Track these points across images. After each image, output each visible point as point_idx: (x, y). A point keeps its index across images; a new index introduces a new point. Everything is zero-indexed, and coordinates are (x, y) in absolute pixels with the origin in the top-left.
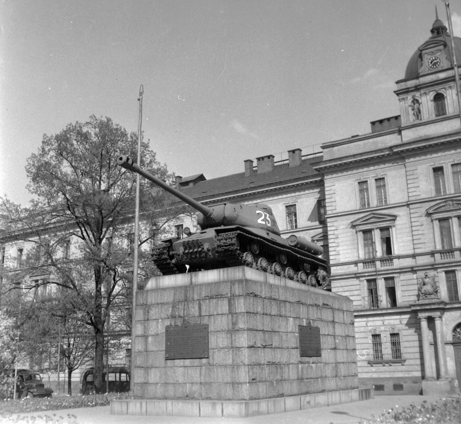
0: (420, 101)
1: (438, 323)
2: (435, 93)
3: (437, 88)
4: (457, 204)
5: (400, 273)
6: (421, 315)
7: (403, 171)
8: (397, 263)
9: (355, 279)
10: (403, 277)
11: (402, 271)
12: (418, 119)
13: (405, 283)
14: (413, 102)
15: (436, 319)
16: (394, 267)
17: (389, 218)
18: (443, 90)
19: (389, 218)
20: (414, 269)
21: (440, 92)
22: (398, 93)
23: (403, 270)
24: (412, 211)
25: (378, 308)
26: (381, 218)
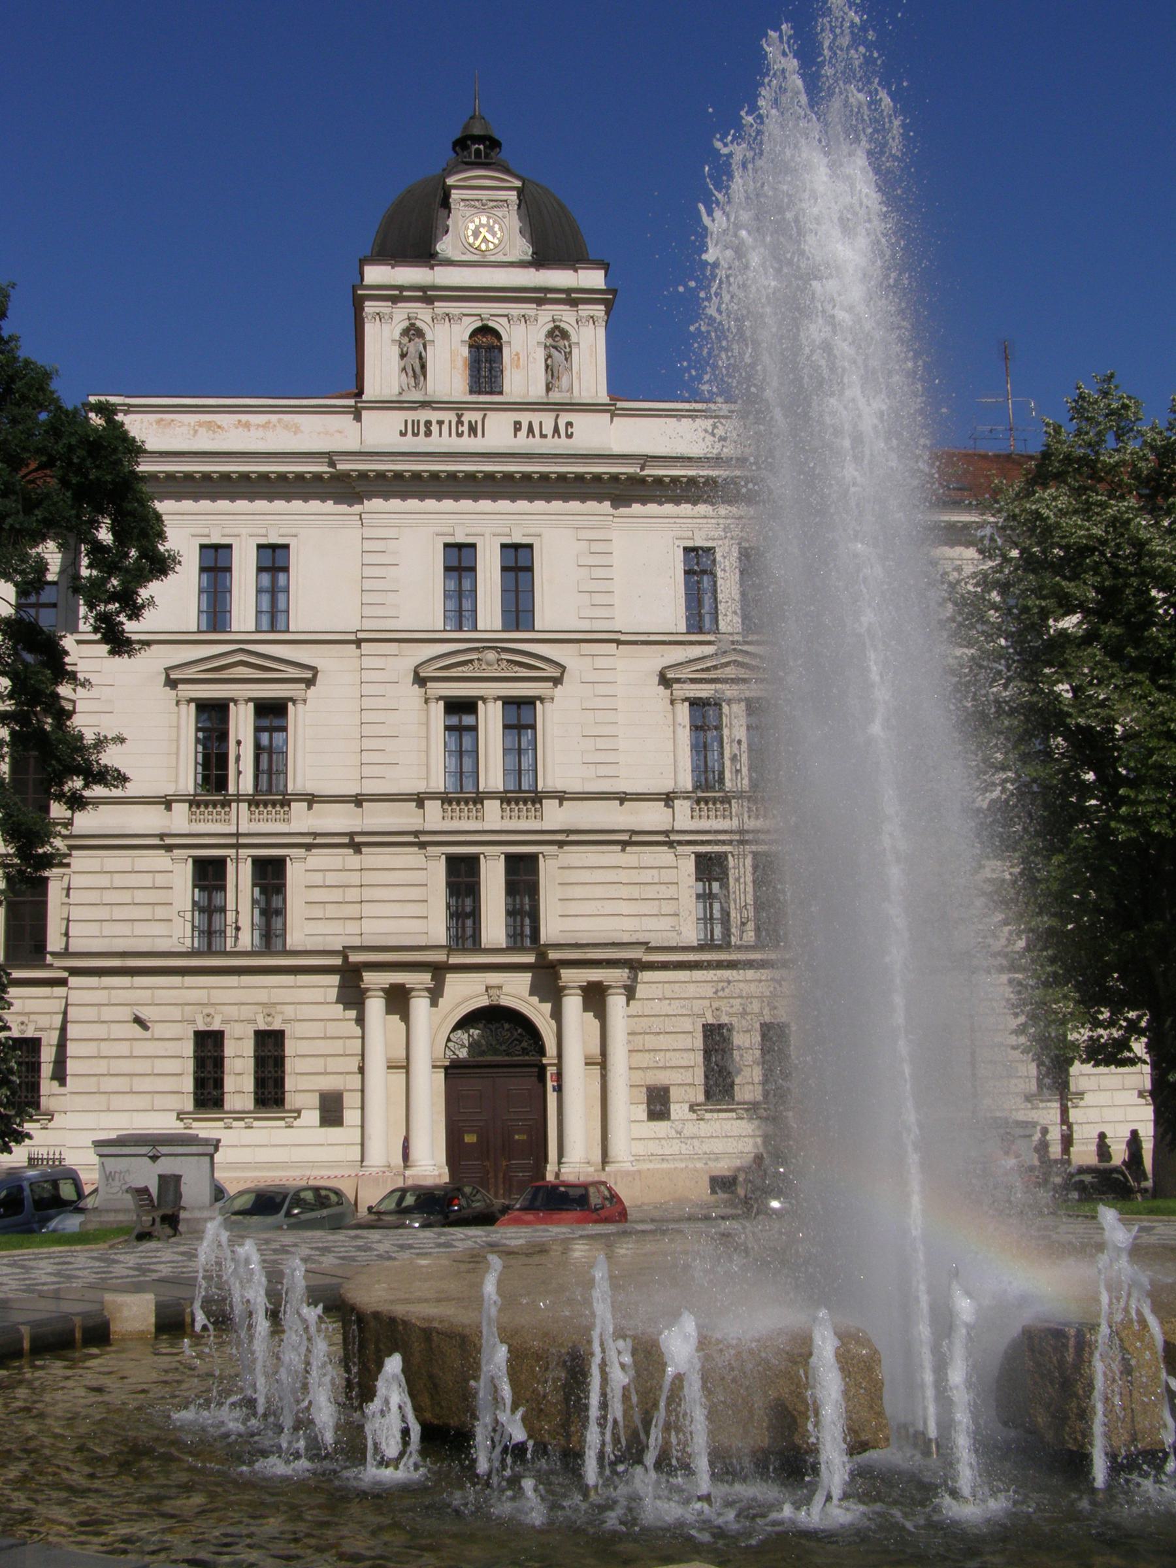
0: (429, 337)
1: (616, 1003)
2: (479, 324)
3: (485, 309)
4: (508, 661)
5: (309, 847)
6: (568, 976)
7: (353, 534)
8: (301, 819)
9: (665, 848)
10: (318, 859)
11: (313, 842)
12: (416, 385)
13: (317, 878)
14: (405, 332)
15: (611, 991)
16: (546, 826)
17: (294, 673)
18: (504, 321)
19: (294, 673)
20: (358, 839)
21: (491, 324)
23: (319, 840)
24: (367, 662)
25: (475, 945)
26: (266, 668)
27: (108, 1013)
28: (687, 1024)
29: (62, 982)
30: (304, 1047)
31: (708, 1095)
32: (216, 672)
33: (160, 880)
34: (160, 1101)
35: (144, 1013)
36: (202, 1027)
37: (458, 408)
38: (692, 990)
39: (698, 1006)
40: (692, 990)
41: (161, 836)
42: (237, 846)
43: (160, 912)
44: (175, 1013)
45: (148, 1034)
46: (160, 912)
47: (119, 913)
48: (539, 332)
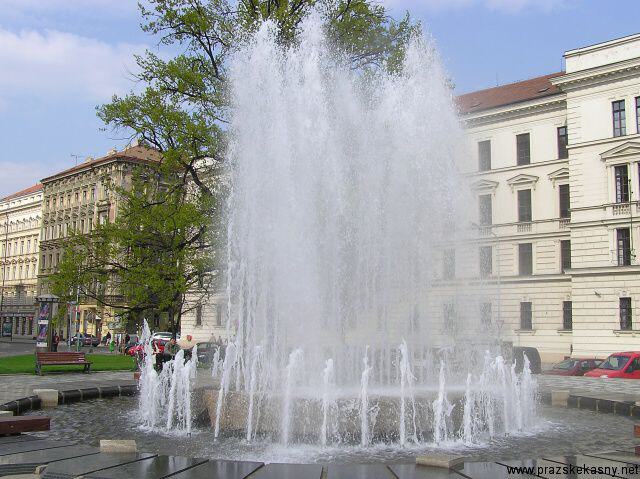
10: (542, 243)
27: (587, 291)
28: (557, 301)
29: (570, 280)
30: (537, 308)
31: (622, 328)
32: (619, 153)
33: (604, 239)
34: (607, 326)
35: (599, 291)
36: (622, 296)
38: (560, 289)
39: (562, 295)
40: (560, 289)
41: (602, 221)
42: (632, 222)
43: (604, 252)
44: (611, 291)
45: (601, 299)
46: (604, 252)
47: (589, 252)
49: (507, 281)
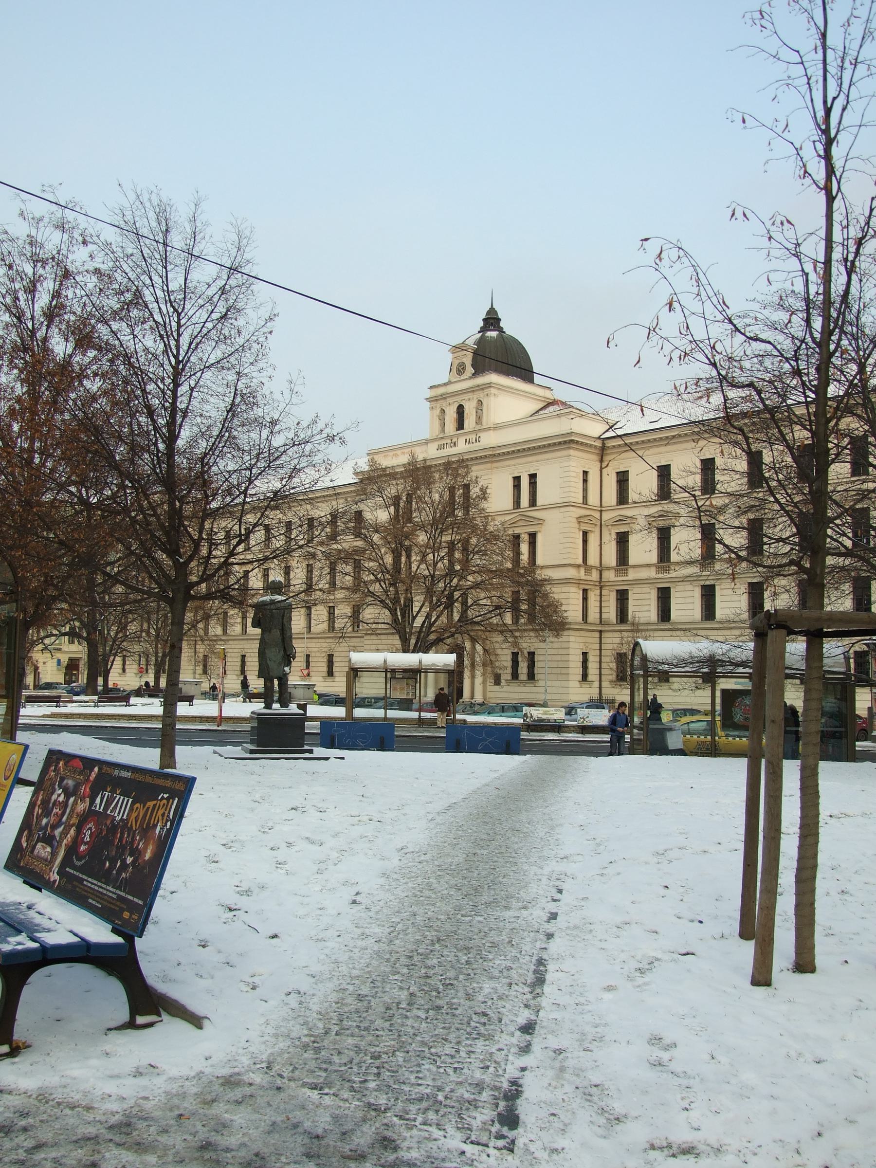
22: (432, 400)
26: (531, 520)
37: (451, 437)
48: (474, 403)
49: (319, 637)
